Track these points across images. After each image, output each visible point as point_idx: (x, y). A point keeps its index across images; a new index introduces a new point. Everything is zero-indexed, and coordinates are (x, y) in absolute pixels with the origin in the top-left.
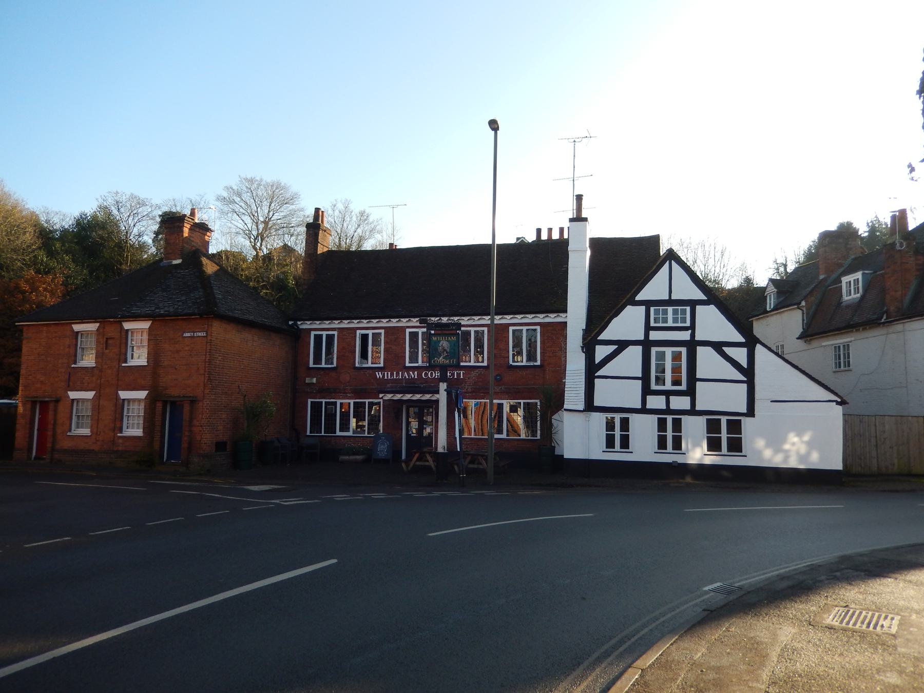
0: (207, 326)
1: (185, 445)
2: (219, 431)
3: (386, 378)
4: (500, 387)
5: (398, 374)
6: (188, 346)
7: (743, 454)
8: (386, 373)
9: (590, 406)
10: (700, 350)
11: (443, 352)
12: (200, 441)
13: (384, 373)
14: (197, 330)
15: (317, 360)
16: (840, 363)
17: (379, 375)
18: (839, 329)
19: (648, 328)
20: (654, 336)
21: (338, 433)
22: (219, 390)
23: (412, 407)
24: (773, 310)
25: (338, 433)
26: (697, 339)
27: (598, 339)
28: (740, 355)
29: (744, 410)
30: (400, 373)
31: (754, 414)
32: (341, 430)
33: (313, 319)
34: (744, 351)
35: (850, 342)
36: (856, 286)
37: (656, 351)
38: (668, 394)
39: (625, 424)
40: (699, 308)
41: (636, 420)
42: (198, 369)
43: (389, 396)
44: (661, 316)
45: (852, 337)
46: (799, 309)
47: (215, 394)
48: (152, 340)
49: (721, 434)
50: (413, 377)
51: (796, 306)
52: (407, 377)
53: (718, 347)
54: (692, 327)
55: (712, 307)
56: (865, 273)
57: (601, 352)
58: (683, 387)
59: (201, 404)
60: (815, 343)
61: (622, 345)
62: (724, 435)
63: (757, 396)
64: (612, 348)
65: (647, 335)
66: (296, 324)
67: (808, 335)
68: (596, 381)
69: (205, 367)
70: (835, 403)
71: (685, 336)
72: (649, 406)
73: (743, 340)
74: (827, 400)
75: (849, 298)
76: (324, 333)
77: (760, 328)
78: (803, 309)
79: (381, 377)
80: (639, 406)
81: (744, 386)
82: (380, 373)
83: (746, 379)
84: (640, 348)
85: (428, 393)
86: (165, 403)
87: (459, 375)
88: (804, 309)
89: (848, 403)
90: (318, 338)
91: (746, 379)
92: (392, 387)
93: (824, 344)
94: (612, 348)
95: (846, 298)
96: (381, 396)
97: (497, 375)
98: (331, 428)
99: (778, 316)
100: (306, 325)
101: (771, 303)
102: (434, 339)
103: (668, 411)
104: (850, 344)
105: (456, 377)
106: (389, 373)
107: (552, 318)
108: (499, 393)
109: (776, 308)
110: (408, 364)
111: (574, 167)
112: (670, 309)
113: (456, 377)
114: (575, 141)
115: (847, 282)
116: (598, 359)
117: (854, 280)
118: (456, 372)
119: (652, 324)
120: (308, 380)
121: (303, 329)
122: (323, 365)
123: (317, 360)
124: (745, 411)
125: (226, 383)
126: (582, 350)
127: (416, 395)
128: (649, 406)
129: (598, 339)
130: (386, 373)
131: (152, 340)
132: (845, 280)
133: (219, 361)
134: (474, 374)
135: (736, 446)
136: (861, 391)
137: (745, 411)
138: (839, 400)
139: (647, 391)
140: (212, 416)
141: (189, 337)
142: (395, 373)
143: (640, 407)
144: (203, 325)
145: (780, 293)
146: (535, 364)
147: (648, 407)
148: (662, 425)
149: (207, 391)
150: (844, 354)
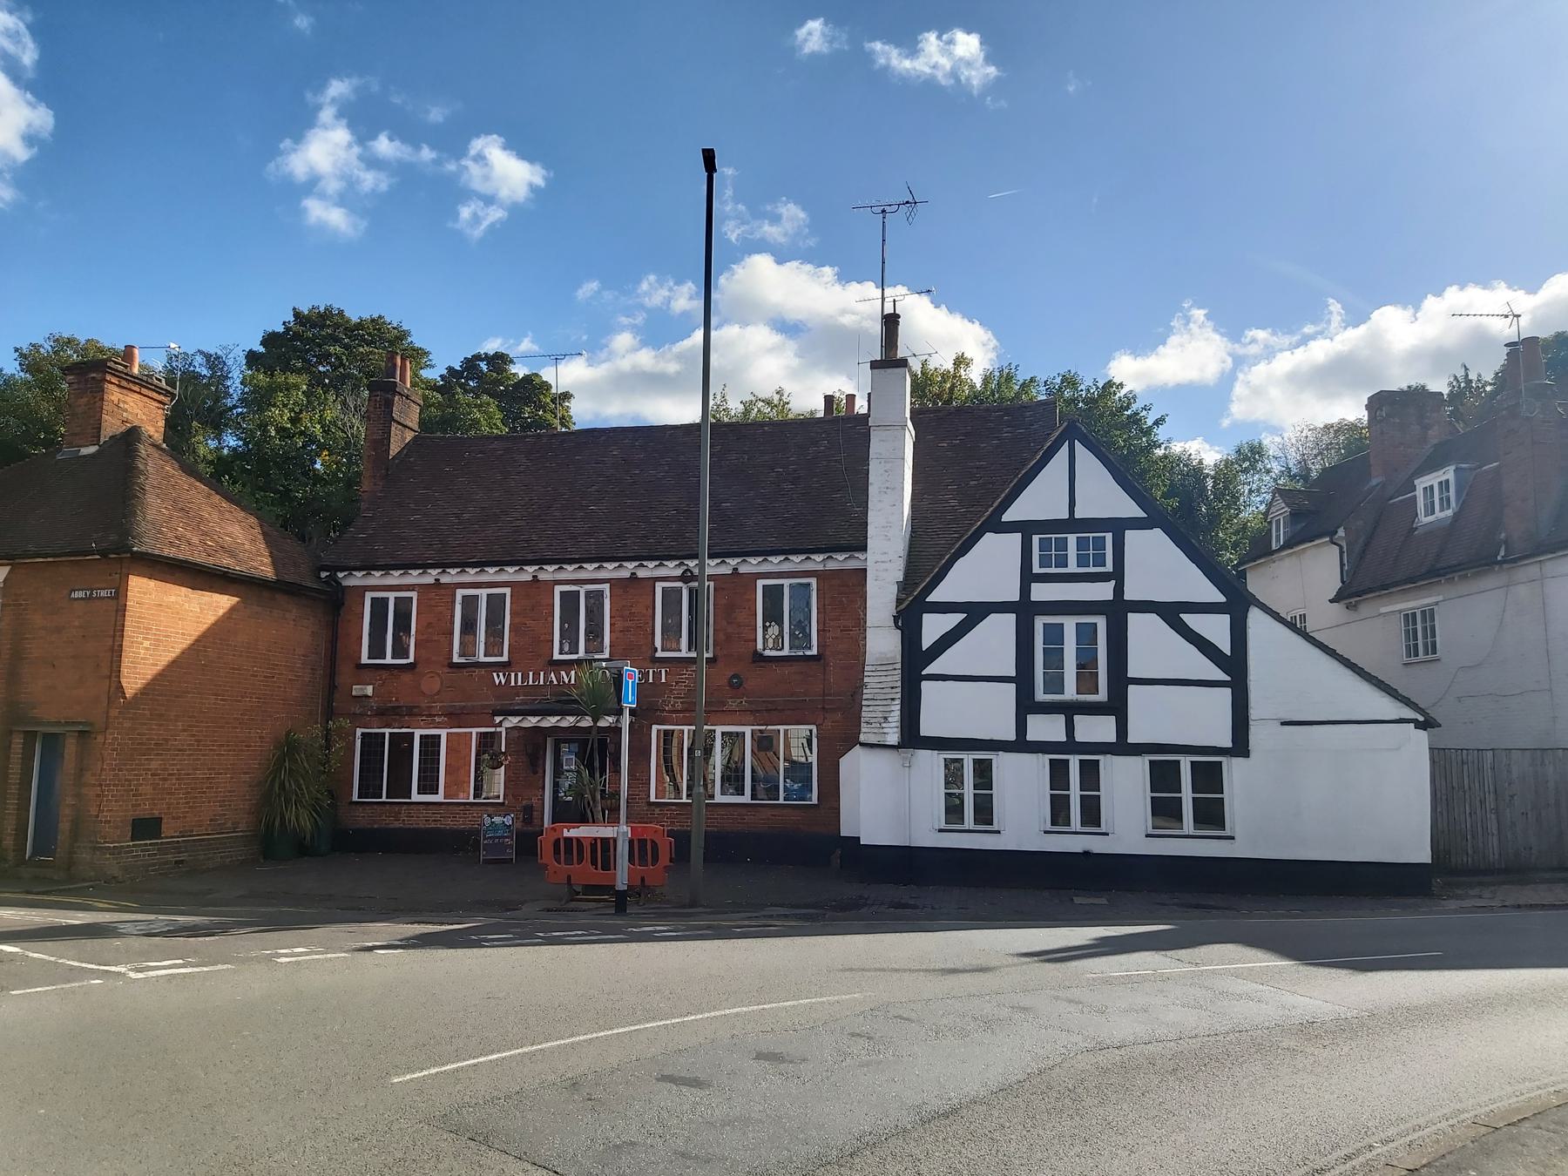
1: (64, 826)
2: (141, 795)
3: (513, 684)
4: (739, 701)
7: (1227, 832)
8: (513, 674)
9: (912, 738)
10: (1133, 619)
12: (97, 816)
13: (509, 675)
15: (377, 649)
16: (1416, 646)
17: (499, 678)
18: (1411, 580)
19: (1028, 578)
20: (1040, 592)
21: (416, 797)
22: (144, 709)
23: (565, 741)
24: (1282, 548)
25: (416, 797)
27: (927, 600)
28: (1216, 629)
29: (1227, 742)
30: (542, 673)
33: (368, 568)
34: (1225, 619)
35: (1437, 603)
36: (1412, 643)
38: (1070, 710)
39: (984, 772)
40: (1130, 535)
41: (1005, 766)
42: (98, 665)
43: (513, 721)
44: (1053, 552)
45: (1439, 595)
46: (1335, 544)
47: (132, 719)
48: (10, 605)
51: (1328, 539)
53: (1172, 613)
54: (1118, 575)
55: (1157, 534)
56: (1461, 469)
57: (934, 627)
58: (1102, 696)
59: (100, 738)
60: (1366, 609)
61: (975, 613)
62: (1187, 795)
63: (1254, 713)
64: (955, 619)
65: (1025, 590)
66: (333, 578)
67: (1350, 594)
69: (112, 662)
70: (1412, 725)
71: (1104, 591)
75: (1431, 518)
76: (392, 596)
77: (1258, 583)
78: (1340, 543)
80: (1011, 735)
81: (1227, 693)
82: (501, 674)
83: (1229, 679)
85: (534, 714)
86: (30, 736)
87: (657, 675)
88: (1344, 544)
89: (1440, 726)
90: (380, 606)
91: (1228, 678)
92: (524, 703)
93: (1383, 610)
94: (955, 619)
95: (1424, 519)
96: (498, 719)
97: (734, 676)
98: (400, 786)
99: (1294, 558)
100: (357, 579)
101: (1278, 537)
103: (1071, 745)
104: (1436, 608)
105: (651, 681)
106: (520, 674)
107: (840, 561)
109: (1288, 545)
111: (883, 263)
112: (1072, 539)
113: (651, 681)
114: (883, 211)
115: (1425, 489)
116: (927, 641)
117: (1441, 483)
118: (651, 671)
119: (1036, 569)
120: (357, 690)
122: (389, 660)
123: (377, 649)
125: (161, 695)
126: (896, 623)
127: (529, 718)
129: (927, 600)
130: (513, 674)
131: (10, 605)
132: (1421, 483)
133: (147, 649)
135: (1211, 815)
136: (1459, 699)
138: (1421, 719)
139: (1026, 706)
140: (125, 765)
143: (1012, 737)
144: (110, 575)
145: (1295, 516)
146: (808, 653)
148: (1058, 774)
149: (114, 712)
150: (1425, 629)
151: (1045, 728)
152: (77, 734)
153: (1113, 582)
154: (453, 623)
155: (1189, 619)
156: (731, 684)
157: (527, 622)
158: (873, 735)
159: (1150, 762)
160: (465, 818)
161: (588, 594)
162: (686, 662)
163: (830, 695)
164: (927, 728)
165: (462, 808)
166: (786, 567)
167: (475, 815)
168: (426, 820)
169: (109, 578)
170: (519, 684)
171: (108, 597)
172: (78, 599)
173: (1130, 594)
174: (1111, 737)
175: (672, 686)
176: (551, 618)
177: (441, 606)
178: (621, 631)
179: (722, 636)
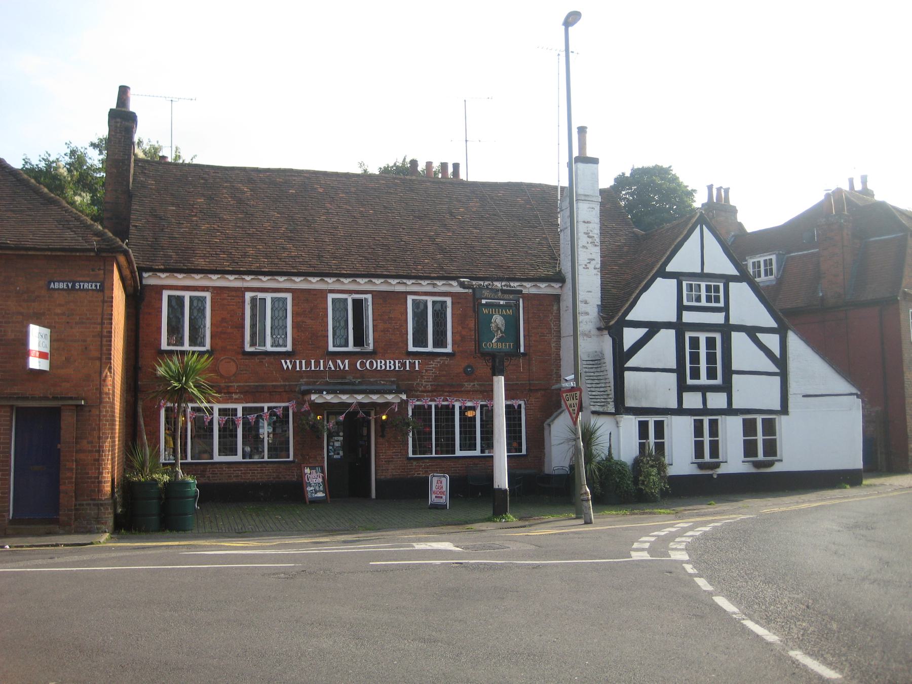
0: (102, 272)
3: (298, 369)
5: (317, 364)
6: (60, 305)
8: (298, 362)
10: (734, 335)
11: (497, 331)
14: (81, 279)
15: (420, 340)
17: (287, 364)
19: (681, 308)
20: (689, 317)
21: (217, 458)
26: (731, 322)
28: (772, 341)
29: (777, 406)
30: (322, 361)
31: (788, 412)
32: (222, 452)
37: (689, 337)
38: (704, 390)
40: (732, 285)
49: (664, 439)
50: (342, 368)
52: (333, 369)
54: (726, 309)
55: (745, 285)
57: (631, 336)
58: (719, 381)
61: (653, 328)
65: (680, 316)
68: (627, 374)
72: (686, 405)
73: (772, 324)
74: (850, 392)
79: (290, 367)
80: (674, 405)
81: (777, 380)
82: (288, 361)
84: (672, 333)
87: (412, 365)
90: (176, 304)
102: (485, 311)
103: (705, 411)
106: (304, 362)
108: (470, 391)
110: (411, 348)
116: (627, 345)
118: (408, 362)
119: (685, 303)
121: (150, 285)
123: (420, 340)
124: (779, 408)
128: (686, 405)
130: (298, 362)
134: (434, 364)
137: (779, 408)
139: (682, 388)
141: (63, 289)
142: (313, 361)
144: (93, 270)
147: (685, 406)
148: (698, 430)
151: (692, 400)
152: (74, 408)
153: (724, 313)
154: (243, 319)
155: (760, 336)
156: (465, 371)
157: (307, 321)
158: (598, 407)
159: (695, 420)
160: (262, 473)
161: (192, 299)
162: (285, 355)
163: (533, 380)
164: (629, 403)
165: (259, 466)
166: (429, 289)
167: (271, 471)
168: (229, 476)
169: (91, 273)
170: (304, 369)
171: (92, 290)
172: (59, 289)
173: (732, 321)
174: (724, 405)
175: (423, 373)
176: (425, 323)
177: (233, 305)
178: (382, 331)
179: (458, 337)
